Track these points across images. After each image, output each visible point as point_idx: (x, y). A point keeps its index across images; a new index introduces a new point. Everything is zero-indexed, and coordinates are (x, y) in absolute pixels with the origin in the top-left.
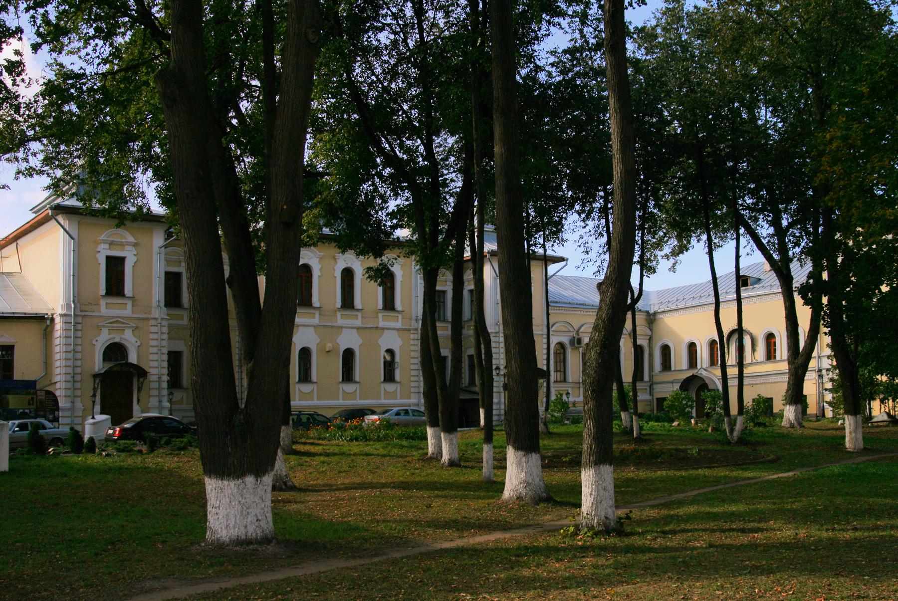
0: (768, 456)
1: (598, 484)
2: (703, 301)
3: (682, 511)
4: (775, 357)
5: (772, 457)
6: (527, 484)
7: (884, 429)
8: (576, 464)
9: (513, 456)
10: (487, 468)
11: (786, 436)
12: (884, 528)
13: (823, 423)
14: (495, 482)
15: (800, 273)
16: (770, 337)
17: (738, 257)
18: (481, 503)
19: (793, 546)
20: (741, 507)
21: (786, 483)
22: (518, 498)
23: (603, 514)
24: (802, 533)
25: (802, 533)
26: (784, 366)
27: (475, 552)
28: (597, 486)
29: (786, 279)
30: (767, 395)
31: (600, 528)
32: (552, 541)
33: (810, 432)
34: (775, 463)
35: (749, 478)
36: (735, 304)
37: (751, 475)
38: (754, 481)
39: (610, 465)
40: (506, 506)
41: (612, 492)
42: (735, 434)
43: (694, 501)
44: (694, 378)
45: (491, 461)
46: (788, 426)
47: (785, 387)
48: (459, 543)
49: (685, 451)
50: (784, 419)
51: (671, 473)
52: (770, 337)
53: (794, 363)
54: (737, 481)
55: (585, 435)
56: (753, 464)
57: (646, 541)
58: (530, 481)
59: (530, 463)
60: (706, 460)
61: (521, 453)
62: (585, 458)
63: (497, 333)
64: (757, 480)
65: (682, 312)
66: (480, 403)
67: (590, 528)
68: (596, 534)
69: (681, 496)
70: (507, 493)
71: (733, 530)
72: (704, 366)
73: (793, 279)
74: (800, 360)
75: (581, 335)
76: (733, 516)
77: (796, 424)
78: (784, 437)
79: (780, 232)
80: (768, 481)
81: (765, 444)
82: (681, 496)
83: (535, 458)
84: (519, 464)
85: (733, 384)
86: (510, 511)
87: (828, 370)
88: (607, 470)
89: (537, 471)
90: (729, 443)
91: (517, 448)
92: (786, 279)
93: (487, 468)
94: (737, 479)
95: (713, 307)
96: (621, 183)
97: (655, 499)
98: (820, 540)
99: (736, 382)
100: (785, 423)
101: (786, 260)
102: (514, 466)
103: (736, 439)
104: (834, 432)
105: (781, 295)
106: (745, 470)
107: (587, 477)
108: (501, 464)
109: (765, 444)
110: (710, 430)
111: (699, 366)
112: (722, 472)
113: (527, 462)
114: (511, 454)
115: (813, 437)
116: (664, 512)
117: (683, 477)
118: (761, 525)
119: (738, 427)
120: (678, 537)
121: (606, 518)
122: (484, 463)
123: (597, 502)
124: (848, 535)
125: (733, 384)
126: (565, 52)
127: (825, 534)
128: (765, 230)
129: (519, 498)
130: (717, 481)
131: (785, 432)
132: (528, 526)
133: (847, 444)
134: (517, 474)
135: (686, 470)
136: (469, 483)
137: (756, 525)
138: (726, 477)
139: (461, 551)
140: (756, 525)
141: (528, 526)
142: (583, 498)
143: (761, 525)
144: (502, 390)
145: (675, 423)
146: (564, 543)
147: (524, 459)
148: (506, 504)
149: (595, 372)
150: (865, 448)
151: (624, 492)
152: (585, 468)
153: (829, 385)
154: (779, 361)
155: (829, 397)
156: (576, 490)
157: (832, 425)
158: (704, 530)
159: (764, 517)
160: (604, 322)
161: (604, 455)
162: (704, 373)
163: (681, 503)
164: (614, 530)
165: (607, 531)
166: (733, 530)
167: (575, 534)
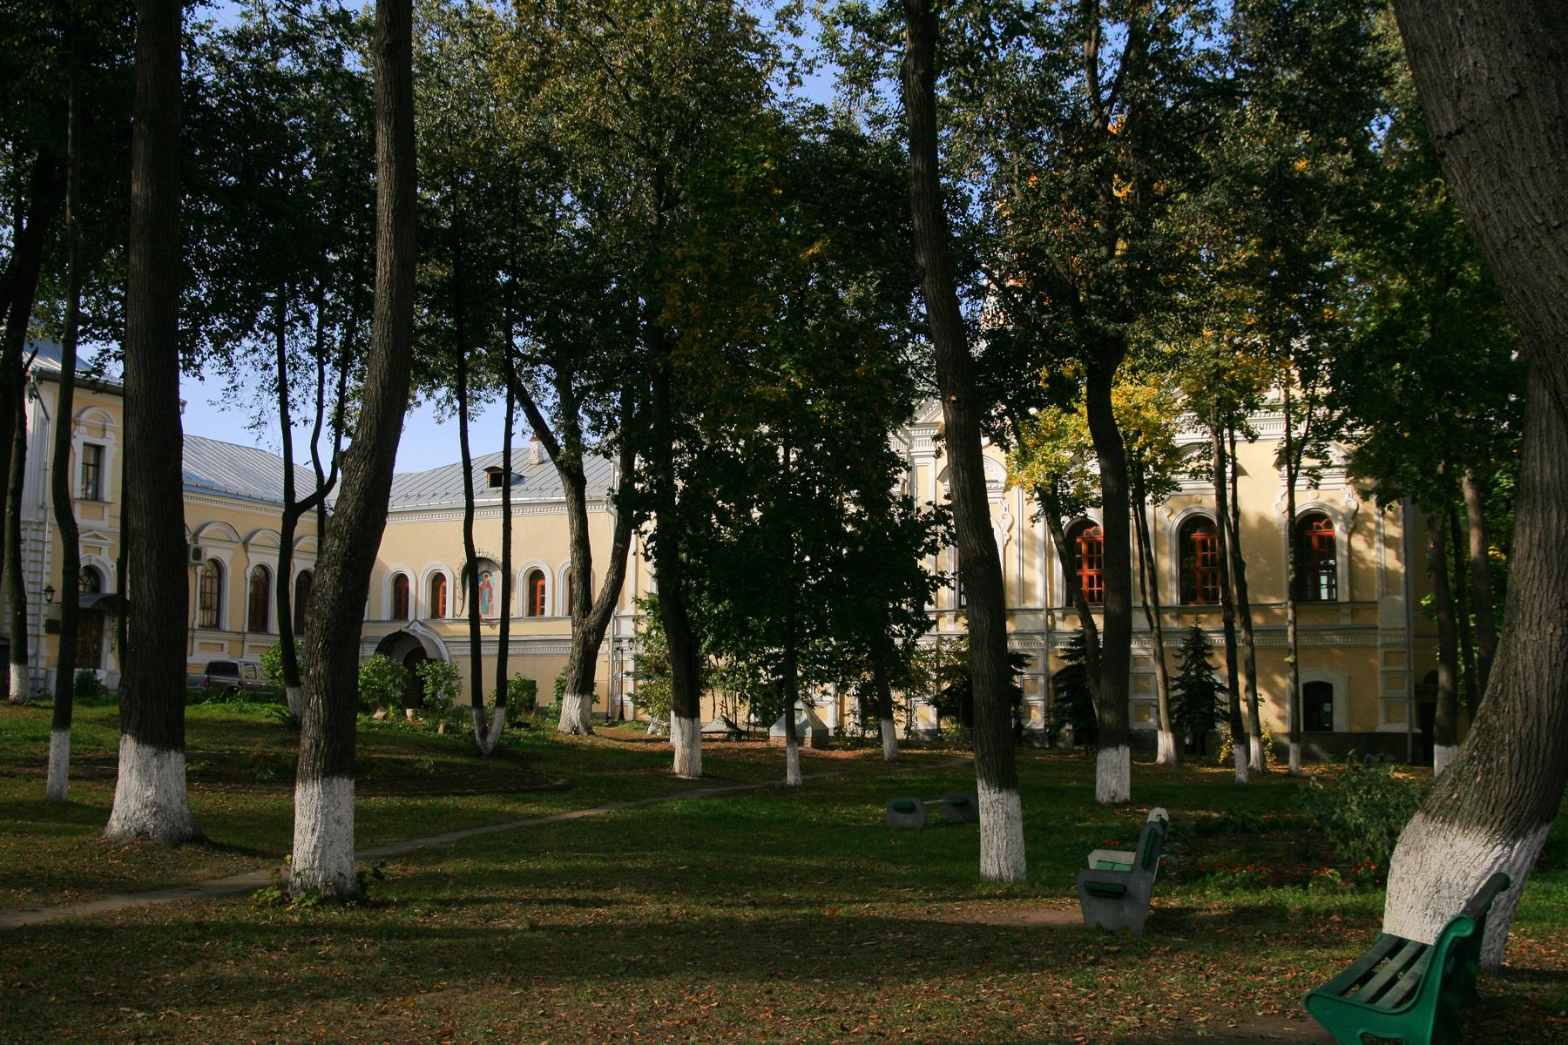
0: (555, 779)
1: (327, 813)
2: (446, 503)
3: (449, 867)
4: (542, 611)
5: (560, 782)
6: (158, 809)
7: (723, 745)
8: (286, 777)
9: (133, 754)
10: (56, 776)
11: (571, 748)
12: (799, 904)
13: (622, 730)
14: (71, 804)
15: (602, 474)
16: (438, 580)
17: (508, 435)
18: (62, 842)
19: (671, 929)
20: (549, 864)
21: (610, 827)
22: (139, 834)
23: (333, 866)
24: (676, 909)
25: (676, 909)
26: (565, 629)
27: (99, 931)
28: (325, 815)
29: (575, 480)
30: (529, 677)
31: (328, 893)
32: (246, 914)
33: (606, 743)
34: (570, 791)
35: (533, 816)
36: (500, 513)
37: (535, 810)
38: (538, 822)
39: (350, 778)
40: (117, 849)
41: (351, 827)
42: (490, 739)
43: (460, 852)
44: (400, 637)
45: (65, 764)
46: (568, 730)
47: (565, 662)
48: (46, 916)
49: (411, 763)
50: (562, 718)
51: (396, 801)
52: (438, 580)
53: (581, 624)
54: (516, 819)
55: (306, 721)
56: (533, 791)
57: (414, 916)
58: (164, 802)
59: (166, 770)
60: (441, 782)
61: (148, 750)
62: (304, 765)
63: (42, 523)
64: (543, 821)
65: (436, 516)
66: (12, 651)
67: (311, 891)
68: (323, 902)
69: (432, 842)
70: (115, 825)
71: (560, 901)
72: (421, 618)
73: (585, 482)
74: (593, 619)
75: (201, 542)
76: (544, 879)
77: (581, 729)
78: (566, 752)
79: (568, 408)
80: (568, 822)
81: (539, 758)
82: (432, 842)
83: (175, 762)
84: (144, 771)
85: (490, 652)
86: (126, 857)
87: (631, 640)
88: (344, 787)
89: (177, 786)
90: (479, 754)
91: (143, 739)
92: (575, 480)
93: (56, 776)
94: (513, 817)
95: (462, 516)
96: (391, 283)
97: (385, 845)
98: (710, 921)
99: (495, 649)
100: (563, 725)
101: (577, 447)
102: (134, 772)
103: (490, 746)
104: (643, 745)
105: (565, 510)
106: (525, 801)
107: (307, 800)
108: (107, 772)
109: (539, 758)
110: (441, 731)
111: (411, 617)
112: (488, 803)
113: (160, 768)
114: (129, 752)
115: (607, 751)
116: (412, 869)
117: (419, 808)
118: (601, 894)
119: (495, 728)
120: (469, 911)
121: (341, 875)
122: (51, 765)
123: (324, 846)
124: (749, 914)
125: (490, 652)
126: (226, 37)
127: (716, 912)
128: (548, 401)
129: (142, 834)
130: (482, 818)
131: (565, 739)
132: (170, 886)
133: (677, 767)
134: (137, 791)
135: (421, 796)
136: (19, 804)
137: (590, 894)
138: (495, 812)
139: (70, 931)
140: (590, 894)
141: (170, 886)
142: (297, 836)
143: (601, 894)
144: (42, 631)
145: (379, 714)
146: (266, 917)
147: (155, 761)
148: (117, 842)
149: (332, 609)
150: (704, 775)
151: (367, 828)
152: (304, 781)
153: (630, 666)
154: (548, 619)
155: (629, 685)
156: (285, 824)
157: (636, 734)
158: (510, 901)
159: (601, 880)
160: (349, 522)
161: (341, 758)
162: (420, 629)
163: (439, 854)
164: (353, 896)
165: (339, 896)
166: (560, 901)
167: (283, 901)
